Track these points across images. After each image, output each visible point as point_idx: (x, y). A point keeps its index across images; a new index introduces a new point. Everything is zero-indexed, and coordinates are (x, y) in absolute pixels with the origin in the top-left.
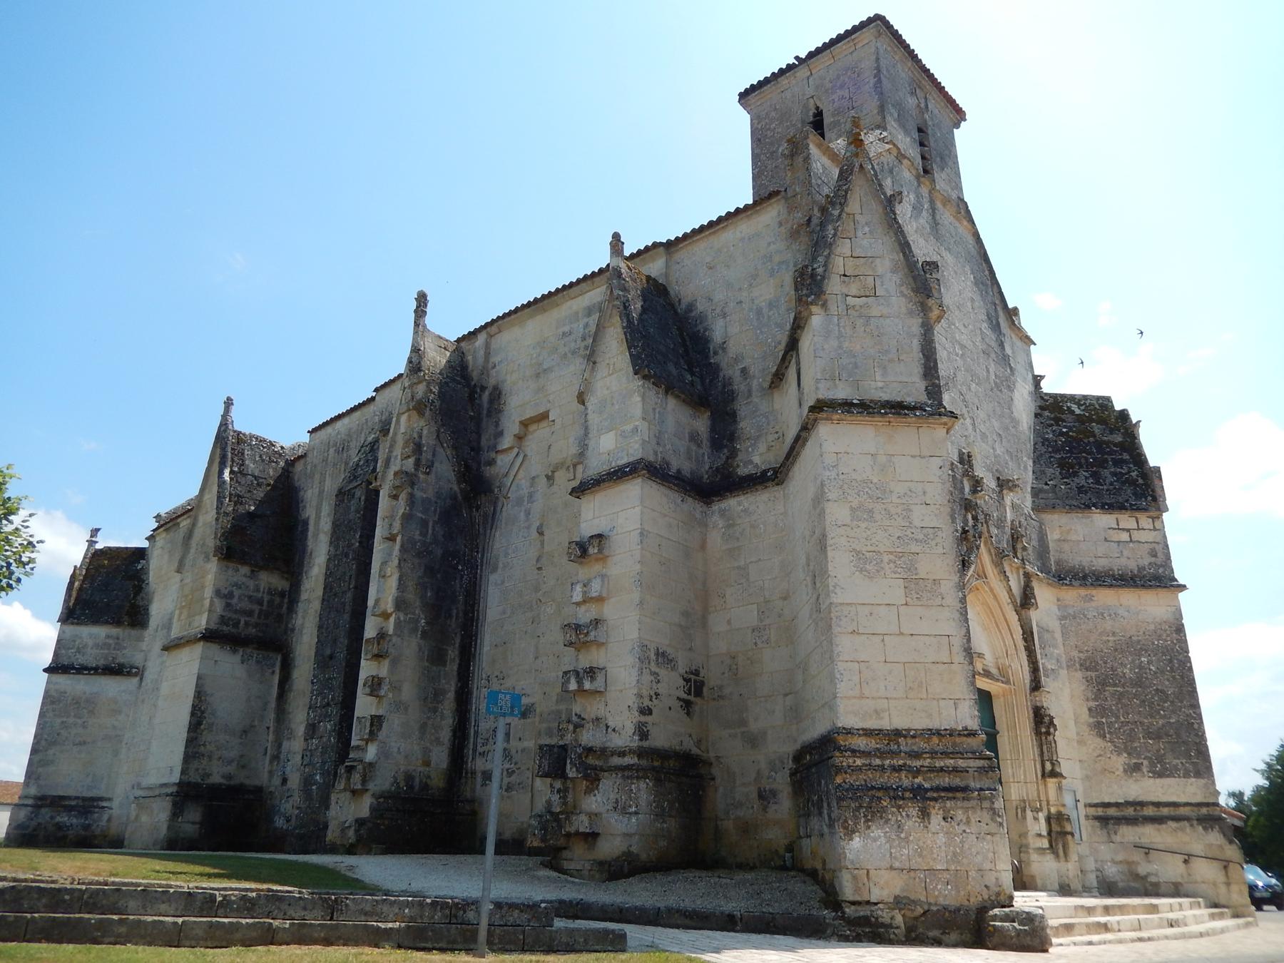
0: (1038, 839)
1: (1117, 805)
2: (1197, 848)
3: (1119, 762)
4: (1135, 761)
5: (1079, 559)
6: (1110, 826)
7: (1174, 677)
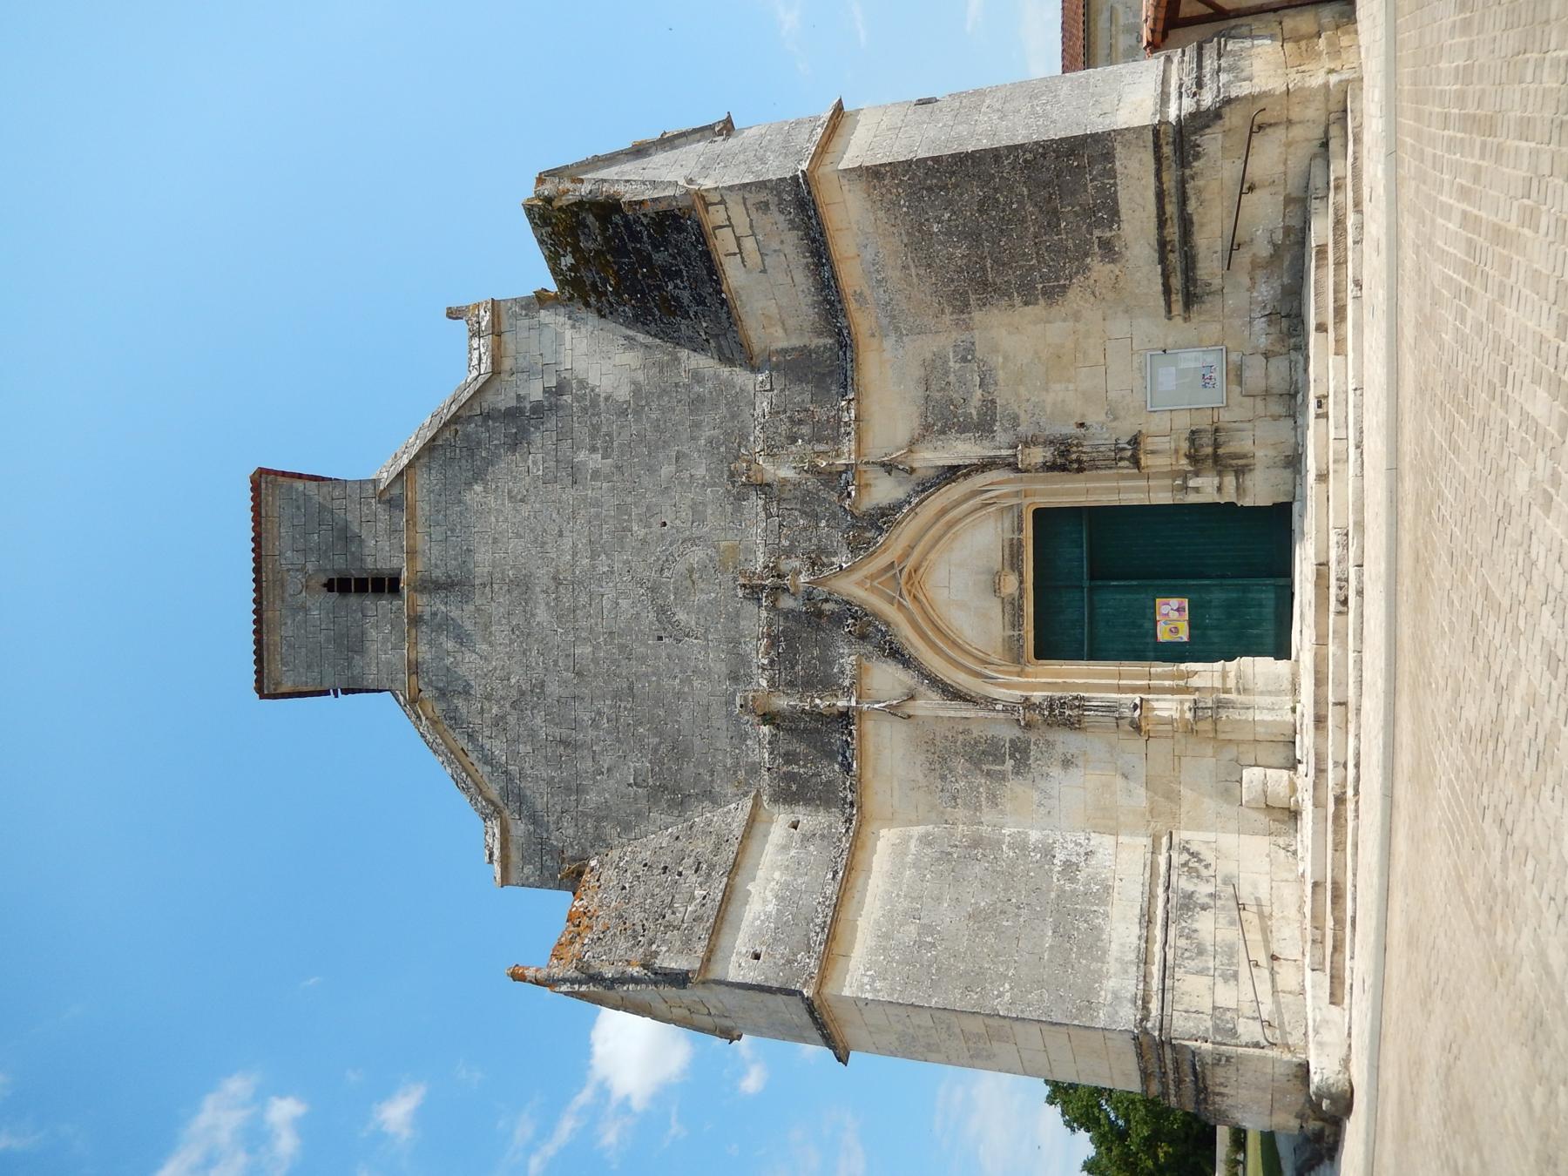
0: (1225, 490)
1: (1166, 276)
2: (1229, 171)
3: (1099, 269)
4: (1096, 246)
5: (805, 308)
6: (1198, 291)
7: (956, 186)
